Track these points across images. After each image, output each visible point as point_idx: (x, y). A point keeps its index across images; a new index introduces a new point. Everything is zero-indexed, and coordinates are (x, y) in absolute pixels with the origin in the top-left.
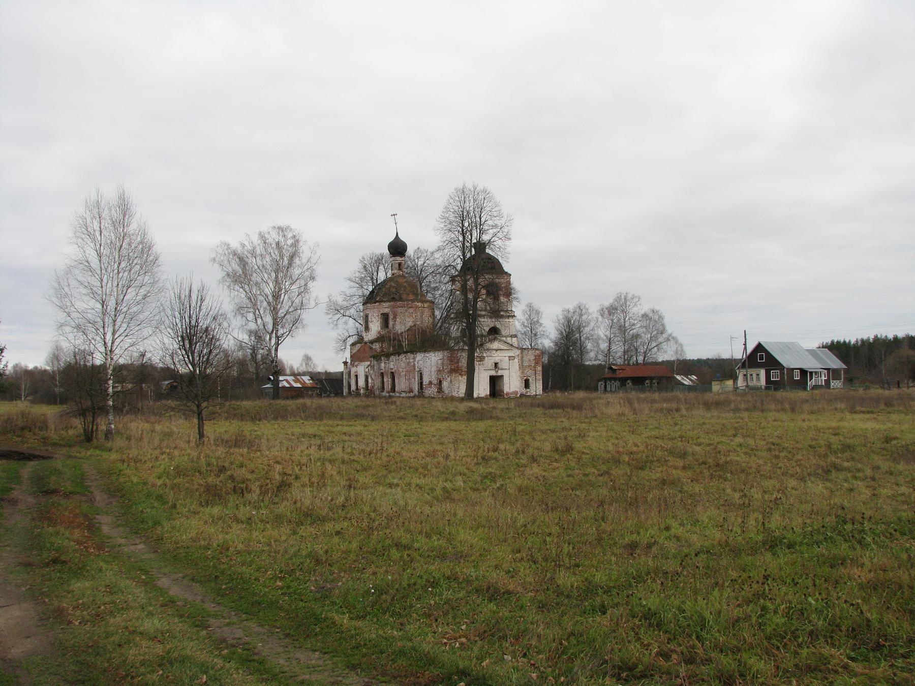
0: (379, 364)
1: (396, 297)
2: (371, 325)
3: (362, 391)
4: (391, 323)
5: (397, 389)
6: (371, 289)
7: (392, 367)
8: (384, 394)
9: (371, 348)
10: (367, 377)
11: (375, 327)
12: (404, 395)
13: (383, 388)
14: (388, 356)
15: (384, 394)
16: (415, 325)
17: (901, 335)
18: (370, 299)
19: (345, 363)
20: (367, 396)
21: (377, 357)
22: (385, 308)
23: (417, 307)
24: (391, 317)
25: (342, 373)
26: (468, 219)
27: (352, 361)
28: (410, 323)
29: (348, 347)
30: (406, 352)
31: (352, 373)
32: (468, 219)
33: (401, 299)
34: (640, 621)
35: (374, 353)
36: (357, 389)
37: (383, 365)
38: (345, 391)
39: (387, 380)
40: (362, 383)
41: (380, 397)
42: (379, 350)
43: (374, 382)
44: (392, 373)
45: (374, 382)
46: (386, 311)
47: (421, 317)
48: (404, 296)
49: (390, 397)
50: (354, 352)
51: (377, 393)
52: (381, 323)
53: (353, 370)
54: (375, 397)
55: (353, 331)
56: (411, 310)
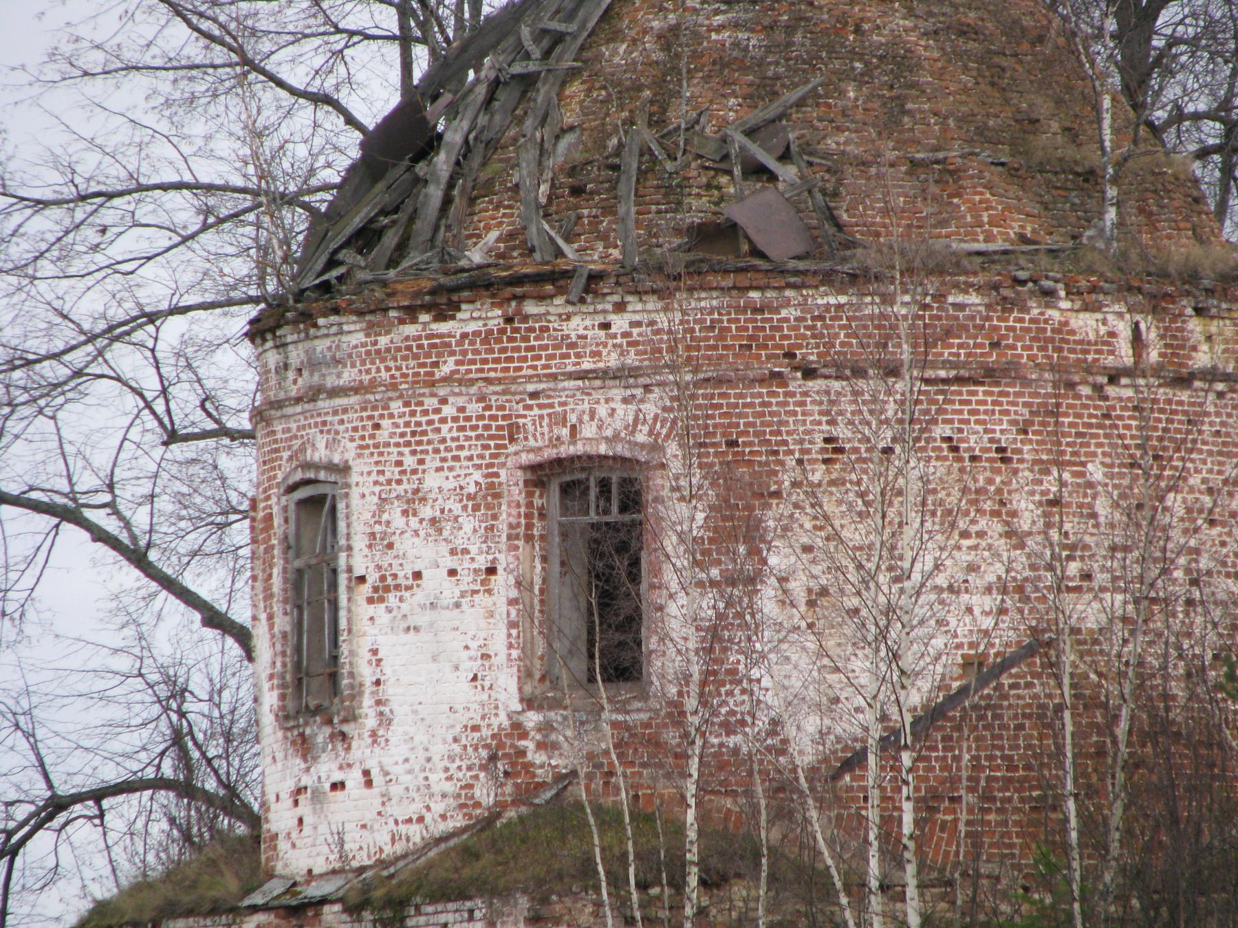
1: (759, 212)
2: (374, 638)
4: (677, 610)
6: (376, 88)
11: (446, 671)
16: (1038, 646)
18: (370, 248)
22: (603, 376)
23: (1074, 371)
24: (679, 516)
28: (959, 611)
33: (830, 254)
34: (621, 107)
46: (604, 422)
47: (1142, 512)
48: (880, 209)
52: (533, 612)
55: (102, 735)
56: (985, 419)
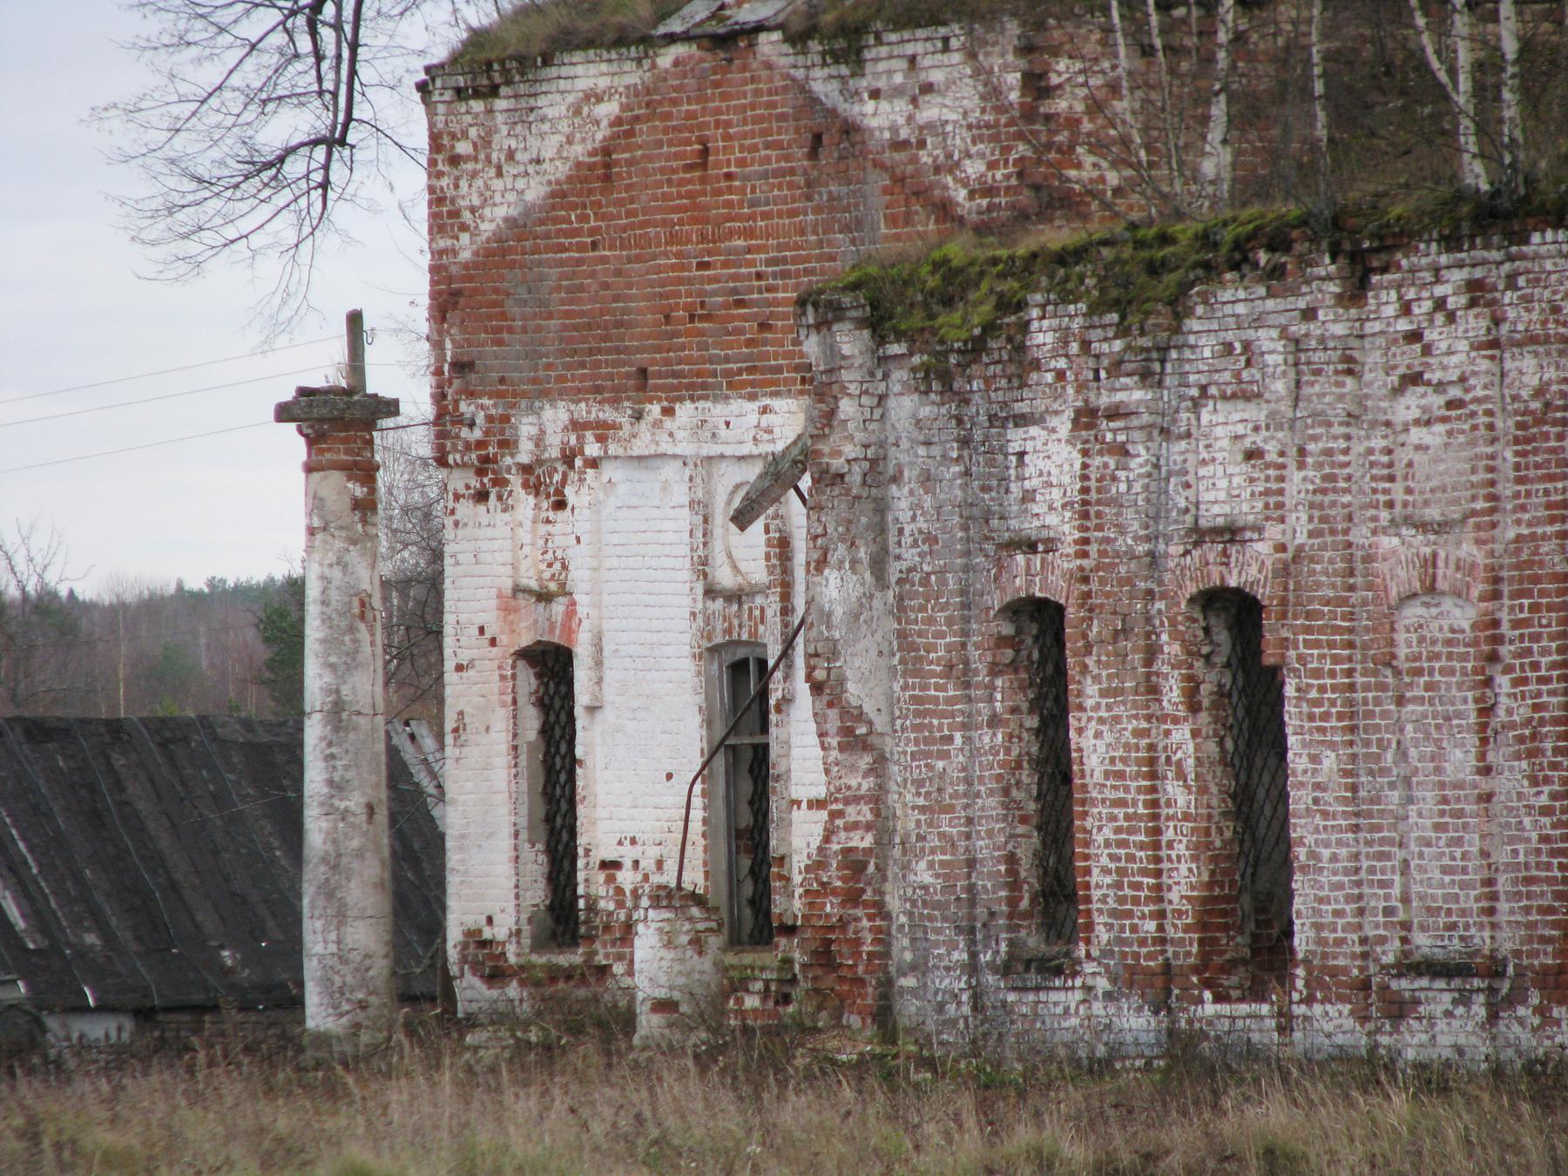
0: (982, 446)
3: (653, 962)
5: (1317, 908)
7: (1222, 490)
8: (1084, 1008)
9: (831, 137)
10: (743, 691)
12: (1446, 1028)
13: (1057, 895)
14: (1148, 283)
15: (1084, 1008)
17: (196, 582)
19: (337, 422)
20: (747, 1046)
21: (939, 312)
25: (278, 614)
26: (284, 413)
27: (456, 375)
29: (396, 115)
30: (1502, 217)
31: (470, 604)
32: (284, 413)
35: (890, 239)
36: (563, 916)
37: (1050, 458)
38: (339, 942)
39: (1137, 744)
40: (644, 794)
41: (999, 1076)
42: (973, 171)
43: (895, 790)
44: (1235, 613)
45: (895, 790)
49: (1191, 1067)
50: (501, 201)
51: (937, 984)
53: (490, 555)
54: (898, 1066)
